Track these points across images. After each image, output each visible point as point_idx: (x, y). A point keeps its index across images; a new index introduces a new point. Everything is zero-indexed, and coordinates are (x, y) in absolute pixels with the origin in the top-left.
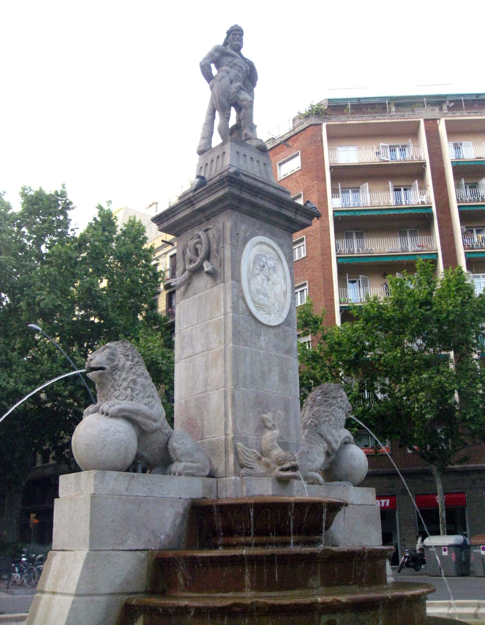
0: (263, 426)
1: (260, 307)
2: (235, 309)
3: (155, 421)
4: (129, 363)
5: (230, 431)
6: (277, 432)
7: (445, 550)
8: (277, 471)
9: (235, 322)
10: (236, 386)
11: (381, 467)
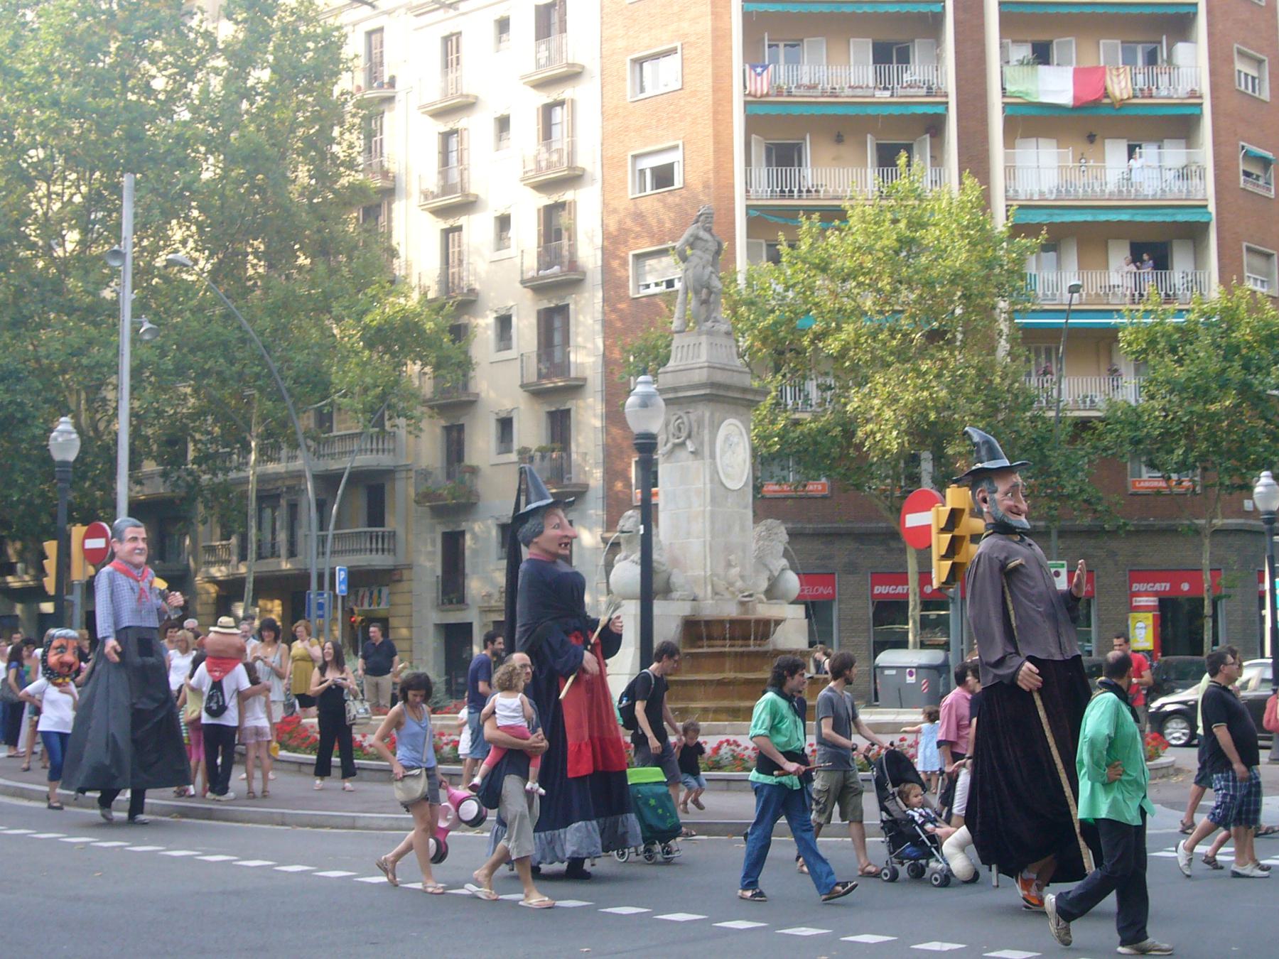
0: (729, 565)
1: (727, 476)
2: (712, 481)
5: (708, 569)
6: (738, 569)
7: (911, 674)
8: (740, 597)
9: (712, 491)
10: (712, 537)
11: (810, 521)
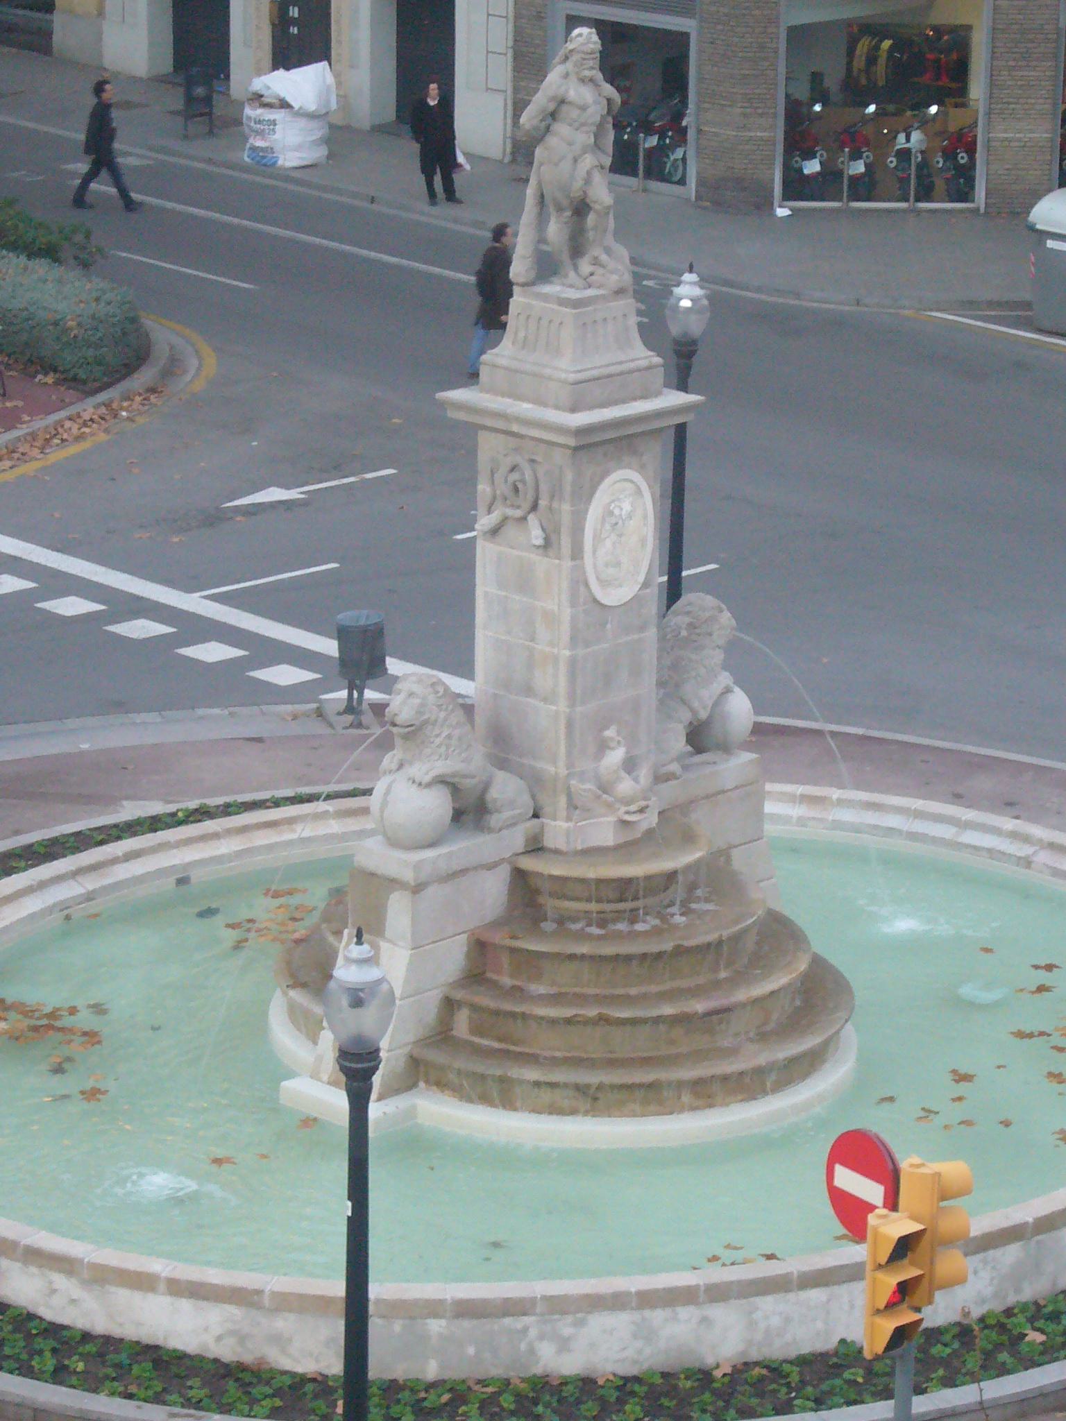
3: (473, 777)
4: (442, 715)
